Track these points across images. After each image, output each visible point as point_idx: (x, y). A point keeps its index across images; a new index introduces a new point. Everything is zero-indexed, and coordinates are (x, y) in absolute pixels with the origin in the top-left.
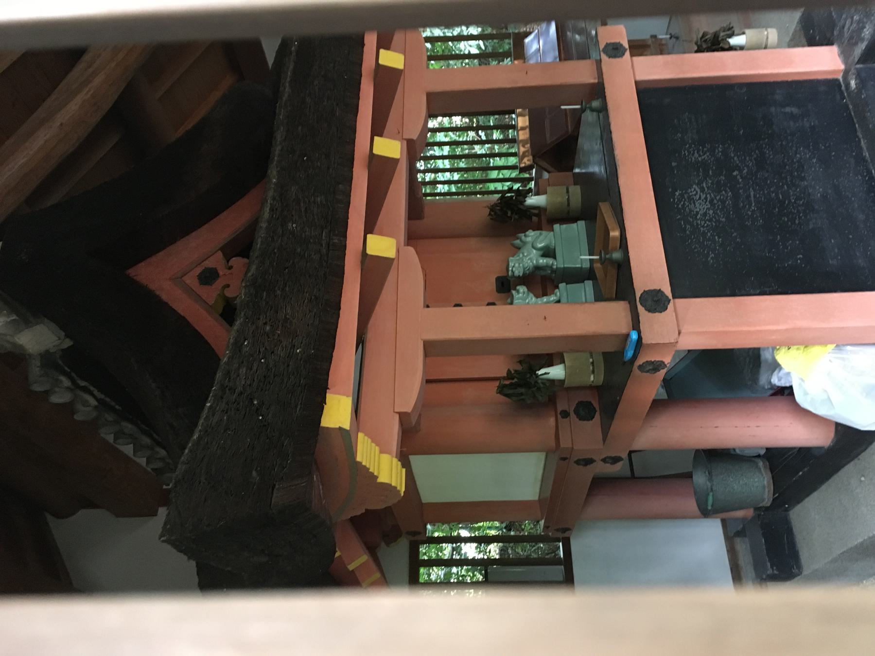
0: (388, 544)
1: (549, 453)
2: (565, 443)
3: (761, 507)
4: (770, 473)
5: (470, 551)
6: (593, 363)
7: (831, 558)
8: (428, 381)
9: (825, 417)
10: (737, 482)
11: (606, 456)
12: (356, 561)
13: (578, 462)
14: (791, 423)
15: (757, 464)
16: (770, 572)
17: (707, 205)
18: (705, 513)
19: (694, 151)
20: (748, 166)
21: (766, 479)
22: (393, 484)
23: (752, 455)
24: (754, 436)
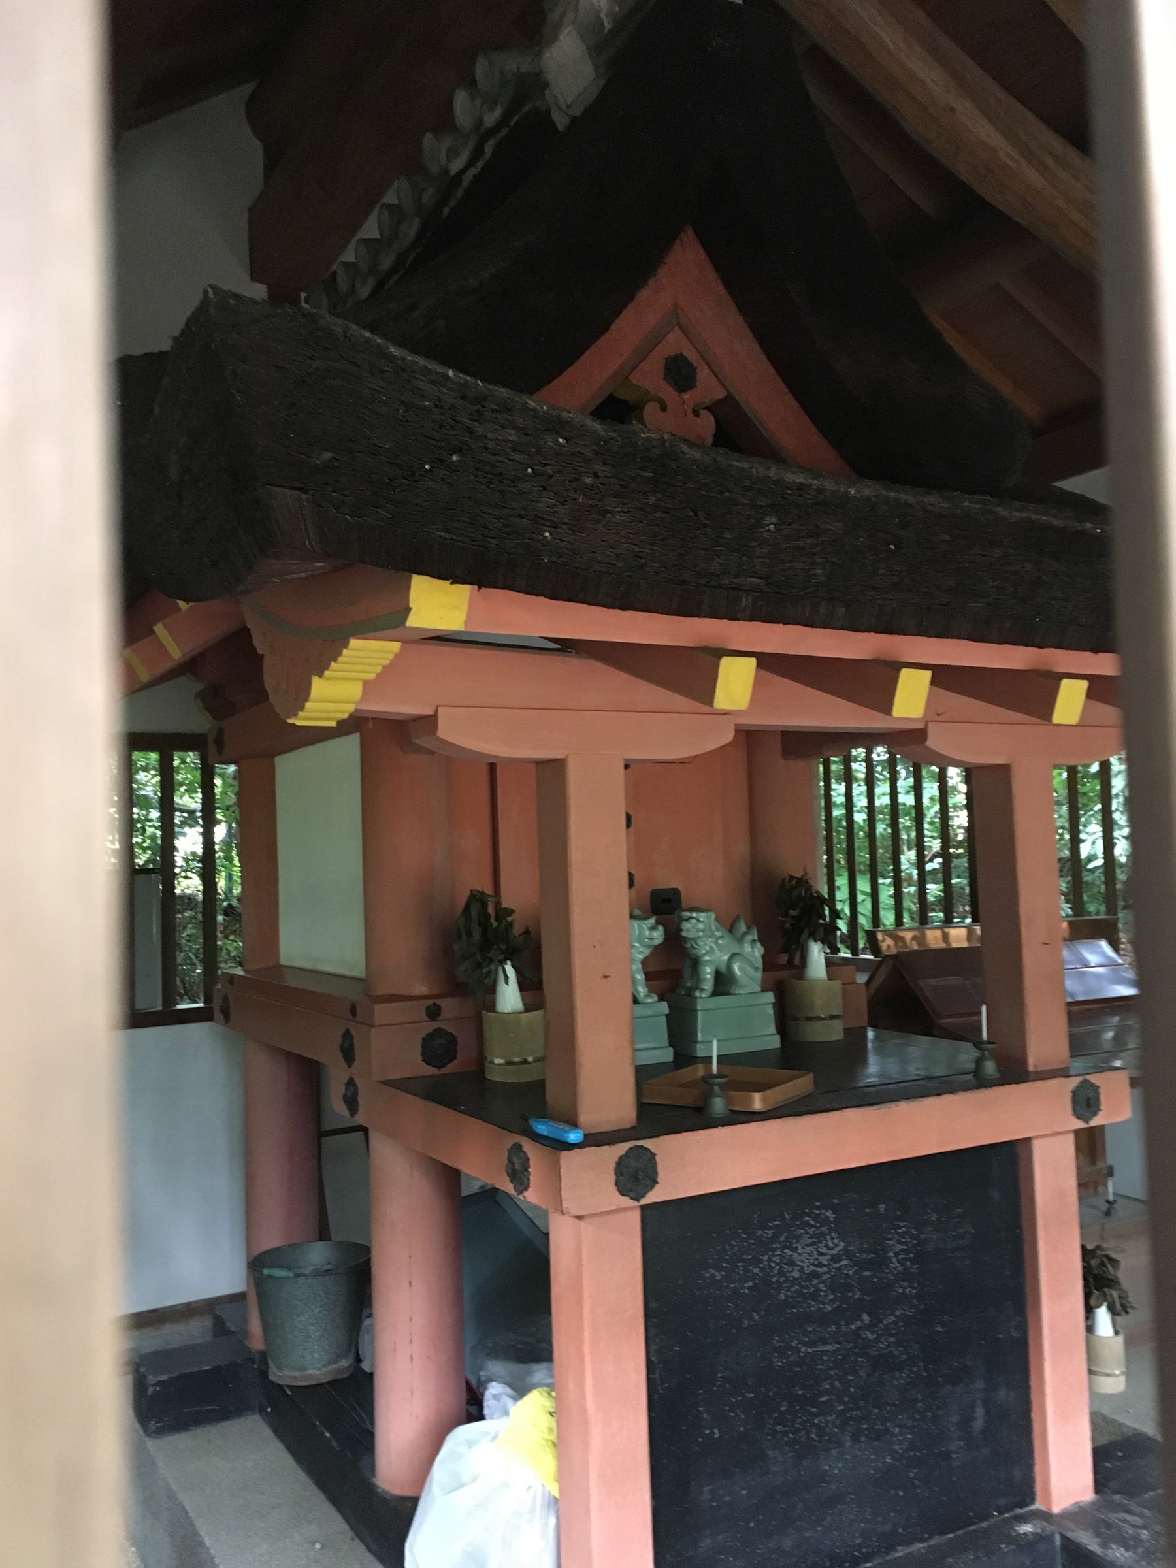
0: (200, 695)
1: (364, 983)
2: (382, 1013)
3: (267, 1363)
5: (189, 842)
6: (525, 1062)
7: (175, 1488)
8: (492, 767)
10: (311, 1321)
11: (359, 1087)
13: (347, 1035)
14: (417, 1418)
15: (345, 1356)
17: (808, 1267)
18: (257, 1264)
19: (906, 1243)
20: (878, 1340)
22: (308, 705)
24: (395, 1352)
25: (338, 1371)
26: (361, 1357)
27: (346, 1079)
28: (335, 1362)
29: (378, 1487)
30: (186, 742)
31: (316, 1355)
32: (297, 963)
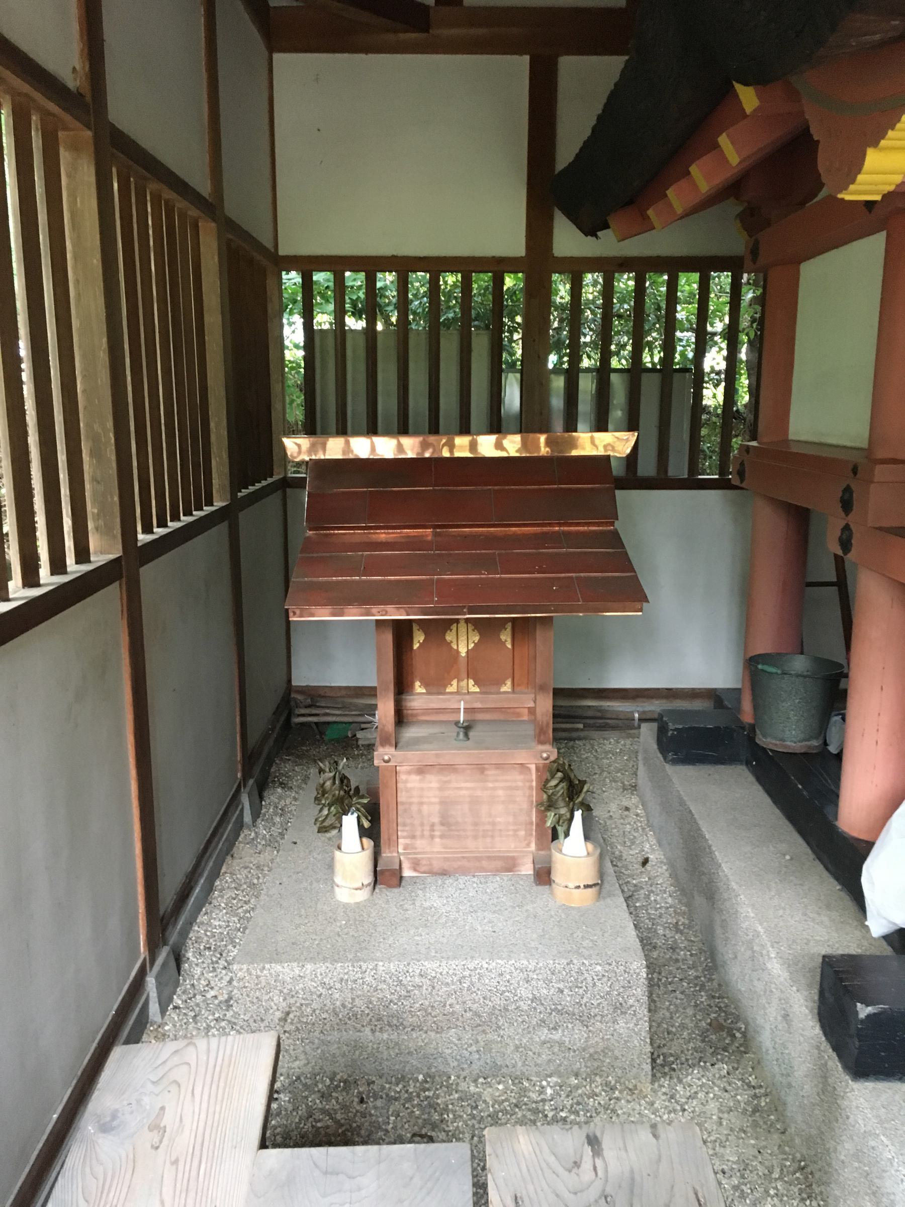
0: (741, 217)
1: (868, 453)
3: (755, 732)
4: (802, 751)
7: (685, 798)
9: (887, 825)
10: (792, 708)
11: (854, 532)
13: (848, 490)
14: (877, 786)
15: (817, 738)
16: (671, 726)
21: (794, 745)
22: (860, 178)
23: (827, 734)
24: (863, 735)
25: (809, 747)
27: (842, 524)
28: (808, 740)
30: (721, 264)
31: (794, 732)
32: (803, 438)
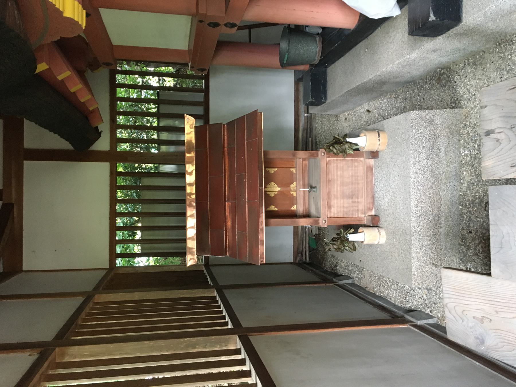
0: (93, 70)
1: (193, 16)
2: (202, 11)
3: (313, 64)
5: (154, 81)
7: (341, 94)
10: (303, 48)
12: (62, 75)
13: (209, 24)
14: (336, 12)
15: (315, 38)
18: (284, 65)
22: (76, 19)
24: (314, 18)
25: (319, 41)
26: (317, 33)
27: (224, 27)
28: (316, 41)
29: (354, 29)
30: (113, 79)
31: (313, 48)
